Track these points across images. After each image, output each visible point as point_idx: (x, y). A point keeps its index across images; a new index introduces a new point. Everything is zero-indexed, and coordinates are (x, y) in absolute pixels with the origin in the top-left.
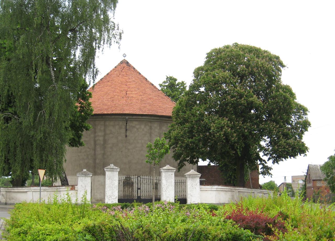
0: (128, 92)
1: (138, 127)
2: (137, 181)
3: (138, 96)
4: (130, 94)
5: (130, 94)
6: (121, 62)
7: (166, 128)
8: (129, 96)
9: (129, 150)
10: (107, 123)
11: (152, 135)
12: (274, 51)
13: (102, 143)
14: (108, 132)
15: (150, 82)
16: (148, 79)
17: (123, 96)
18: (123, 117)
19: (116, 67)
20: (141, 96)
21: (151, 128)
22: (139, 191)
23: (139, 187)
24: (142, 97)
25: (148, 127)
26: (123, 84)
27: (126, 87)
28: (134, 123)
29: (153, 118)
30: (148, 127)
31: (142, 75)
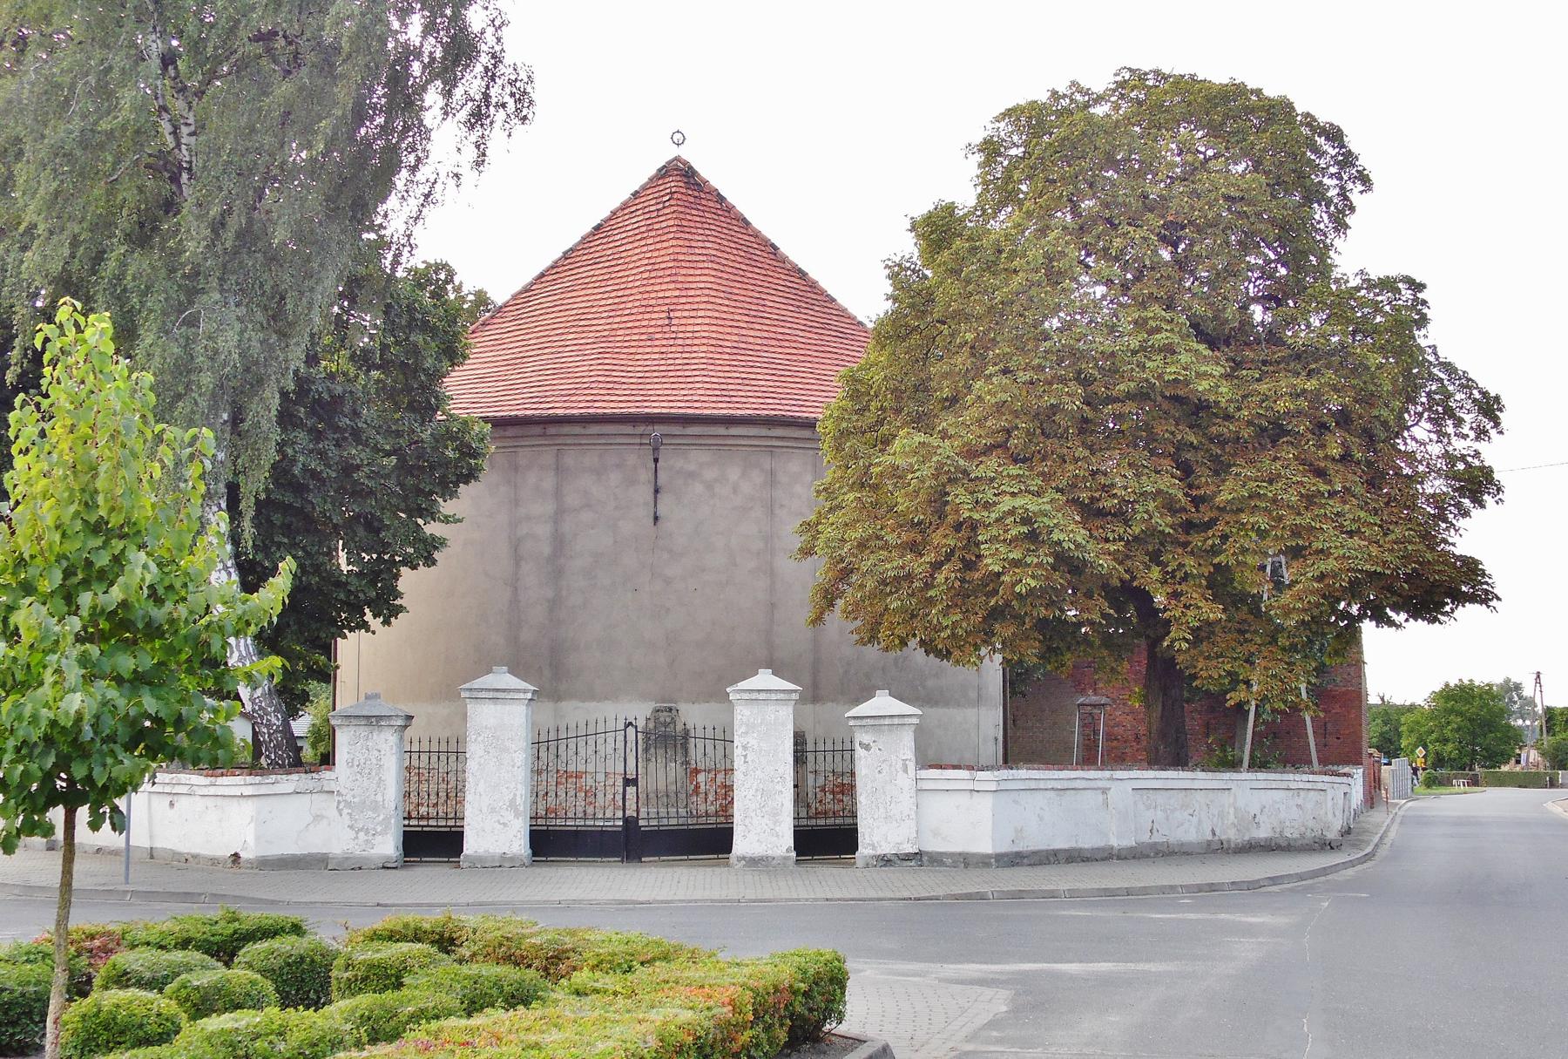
0: (678, 314)
1: (709, 474)
2: (620, 744)
3: (721, 329)
4: (683, 321)
5: (683, 321)
6: (660, 170)
7: (801, 484)
8: (682, 328)
9: (668, 581)
10: (570, 459)
11: (777, 511)
12: (1312, 100)
13: (547, 550)
14: (572, 500)
15: (791, 263)
16: (785, 248)
17: (651, 330)
18: (640, 429)
19: (636, 194)
20: (735, 331)
21: (772, 480)
22: (631, 790)
23: (631, 775)
24: (744, 332)
25: (757, 477)
26: (661, 273)
27: (672, 286)
28: (696, 459)
29: (779, 432)
30: (757, 477)
31: (754, 230)
